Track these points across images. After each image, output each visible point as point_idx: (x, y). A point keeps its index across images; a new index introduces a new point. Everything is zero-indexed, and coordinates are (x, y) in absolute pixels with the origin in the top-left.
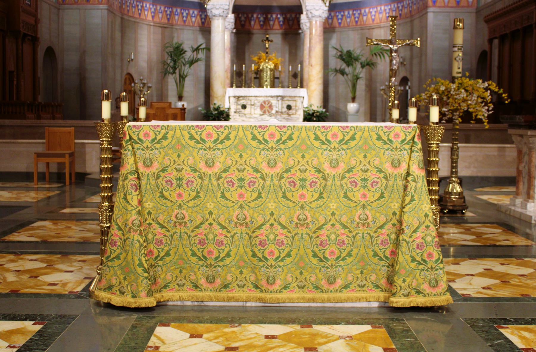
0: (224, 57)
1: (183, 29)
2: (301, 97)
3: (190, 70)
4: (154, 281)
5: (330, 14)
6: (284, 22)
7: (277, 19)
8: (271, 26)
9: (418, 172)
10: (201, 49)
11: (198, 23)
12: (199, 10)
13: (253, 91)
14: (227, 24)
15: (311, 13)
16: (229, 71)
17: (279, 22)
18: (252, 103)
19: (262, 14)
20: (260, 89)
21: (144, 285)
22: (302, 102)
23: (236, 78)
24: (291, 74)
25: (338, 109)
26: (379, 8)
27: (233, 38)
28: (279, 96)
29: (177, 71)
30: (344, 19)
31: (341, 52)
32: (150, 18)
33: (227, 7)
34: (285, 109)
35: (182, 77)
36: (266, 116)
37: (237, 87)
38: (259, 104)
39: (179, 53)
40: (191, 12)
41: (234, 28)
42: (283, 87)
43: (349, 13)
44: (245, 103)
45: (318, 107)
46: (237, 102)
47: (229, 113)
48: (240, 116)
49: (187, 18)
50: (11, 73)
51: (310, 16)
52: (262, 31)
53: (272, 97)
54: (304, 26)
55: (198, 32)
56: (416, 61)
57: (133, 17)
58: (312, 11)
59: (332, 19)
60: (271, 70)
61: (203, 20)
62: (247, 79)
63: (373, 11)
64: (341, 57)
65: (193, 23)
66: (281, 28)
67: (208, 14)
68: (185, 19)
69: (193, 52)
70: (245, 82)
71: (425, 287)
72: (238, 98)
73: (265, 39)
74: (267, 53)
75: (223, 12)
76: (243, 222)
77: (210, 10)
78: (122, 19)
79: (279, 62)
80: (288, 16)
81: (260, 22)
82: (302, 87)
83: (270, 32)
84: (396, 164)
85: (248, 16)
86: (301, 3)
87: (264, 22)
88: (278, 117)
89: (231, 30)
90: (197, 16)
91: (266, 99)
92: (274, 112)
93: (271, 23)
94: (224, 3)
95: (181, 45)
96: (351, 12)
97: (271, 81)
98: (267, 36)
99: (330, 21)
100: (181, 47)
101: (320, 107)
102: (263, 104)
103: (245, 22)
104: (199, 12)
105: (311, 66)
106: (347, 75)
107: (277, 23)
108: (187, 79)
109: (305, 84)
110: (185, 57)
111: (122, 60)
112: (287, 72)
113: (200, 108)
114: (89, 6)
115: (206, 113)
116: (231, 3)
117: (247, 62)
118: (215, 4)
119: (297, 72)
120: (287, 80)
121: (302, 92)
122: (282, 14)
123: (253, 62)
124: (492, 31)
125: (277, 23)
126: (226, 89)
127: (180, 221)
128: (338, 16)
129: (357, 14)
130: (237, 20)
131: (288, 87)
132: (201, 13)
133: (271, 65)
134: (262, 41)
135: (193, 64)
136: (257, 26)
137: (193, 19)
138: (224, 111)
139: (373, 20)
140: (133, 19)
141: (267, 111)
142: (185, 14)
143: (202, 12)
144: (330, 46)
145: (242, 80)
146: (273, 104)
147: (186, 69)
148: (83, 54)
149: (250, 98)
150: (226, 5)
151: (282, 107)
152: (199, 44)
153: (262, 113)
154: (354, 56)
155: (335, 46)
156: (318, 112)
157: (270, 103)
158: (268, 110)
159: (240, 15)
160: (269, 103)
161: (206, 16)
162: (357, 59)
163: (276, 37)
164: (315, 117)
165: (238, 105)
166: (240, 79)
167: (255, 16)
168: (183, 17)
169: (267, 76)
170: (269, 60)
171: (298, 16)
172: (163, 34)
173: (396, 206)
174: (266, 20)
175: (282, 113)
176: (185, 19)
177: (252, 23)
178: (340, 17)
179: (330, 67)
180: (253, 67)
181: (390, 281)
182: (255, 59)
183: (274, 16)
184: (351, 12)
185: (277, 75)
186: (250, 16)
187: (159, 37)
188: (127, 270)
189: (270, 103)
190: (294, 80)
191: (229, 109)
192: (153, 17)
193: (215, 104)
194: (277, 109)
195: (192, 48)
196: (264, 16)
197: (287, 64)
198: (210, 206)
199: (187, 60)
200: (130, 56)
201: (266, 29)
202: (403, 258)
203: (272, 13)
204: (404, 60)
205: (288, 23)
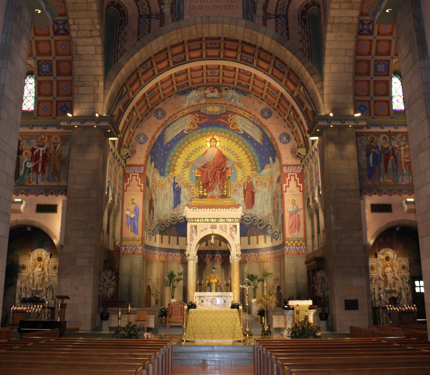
4: (194, 336)
6: (222, 258)
7: (218, 257)
9: (238, 317)
13: (207, 294)
17: (219, 258)
19: (211, 254)
20: (211, 293)
21: (192, 337)
29: (171, 284)
32: (158, 258)
42: (221, 291)
50: (405, 347)
52: (211, 263)
53: (216, 296)
56: (282, 279)
57: (151, 258)
59: (245, 257)
60: (216, 283)
63: (264, 253)
64: (248, 277)
66: (221, 261)
71: (239, 337)
72: (200, 297)
76: (209, 326)
78: (147, 260)
80: (224, 255)
82: (231, 291)
83: (215, 263)
84: (234, 316)
87: (212, 258)
91: (214, 297)
93: (216, 259)
103: (203, 258)
107: (218, 258)
108: (176, 289)
111: (146, 279)
114: (134, 256)
121: (231, 294)
122: (221, 254)
123: (207, 279)
124: (308, 268)
125: (218, 258)
127: (198, 326)
129: (257, 254)
130: (199, 257)
133: (215, 281)
136: (209, 260)
137: (178, 258)
139: (264, 258)
140: (150, 260)
142: (174, 255)
147: (175, 284)
148: (131, 277)
162: (256, 278)
163: (218, 266)
165: (200, 300)
167: (208, 255)
169: (214, 286)
170: (215, 278)
172: (163, 266)
173: (234, 323)
174: (213, 257)
177: (206, 259)
180: (207, 282)
181: (234, 336)
182: (208, 278)
183: (217, 255)
187: (162, 267)
188: (190, 334)
192: (159, 258)
198: (203, 324)
200: (149, 277)
201: (213, 262)
202: (236, 332)
204: (278, 278)
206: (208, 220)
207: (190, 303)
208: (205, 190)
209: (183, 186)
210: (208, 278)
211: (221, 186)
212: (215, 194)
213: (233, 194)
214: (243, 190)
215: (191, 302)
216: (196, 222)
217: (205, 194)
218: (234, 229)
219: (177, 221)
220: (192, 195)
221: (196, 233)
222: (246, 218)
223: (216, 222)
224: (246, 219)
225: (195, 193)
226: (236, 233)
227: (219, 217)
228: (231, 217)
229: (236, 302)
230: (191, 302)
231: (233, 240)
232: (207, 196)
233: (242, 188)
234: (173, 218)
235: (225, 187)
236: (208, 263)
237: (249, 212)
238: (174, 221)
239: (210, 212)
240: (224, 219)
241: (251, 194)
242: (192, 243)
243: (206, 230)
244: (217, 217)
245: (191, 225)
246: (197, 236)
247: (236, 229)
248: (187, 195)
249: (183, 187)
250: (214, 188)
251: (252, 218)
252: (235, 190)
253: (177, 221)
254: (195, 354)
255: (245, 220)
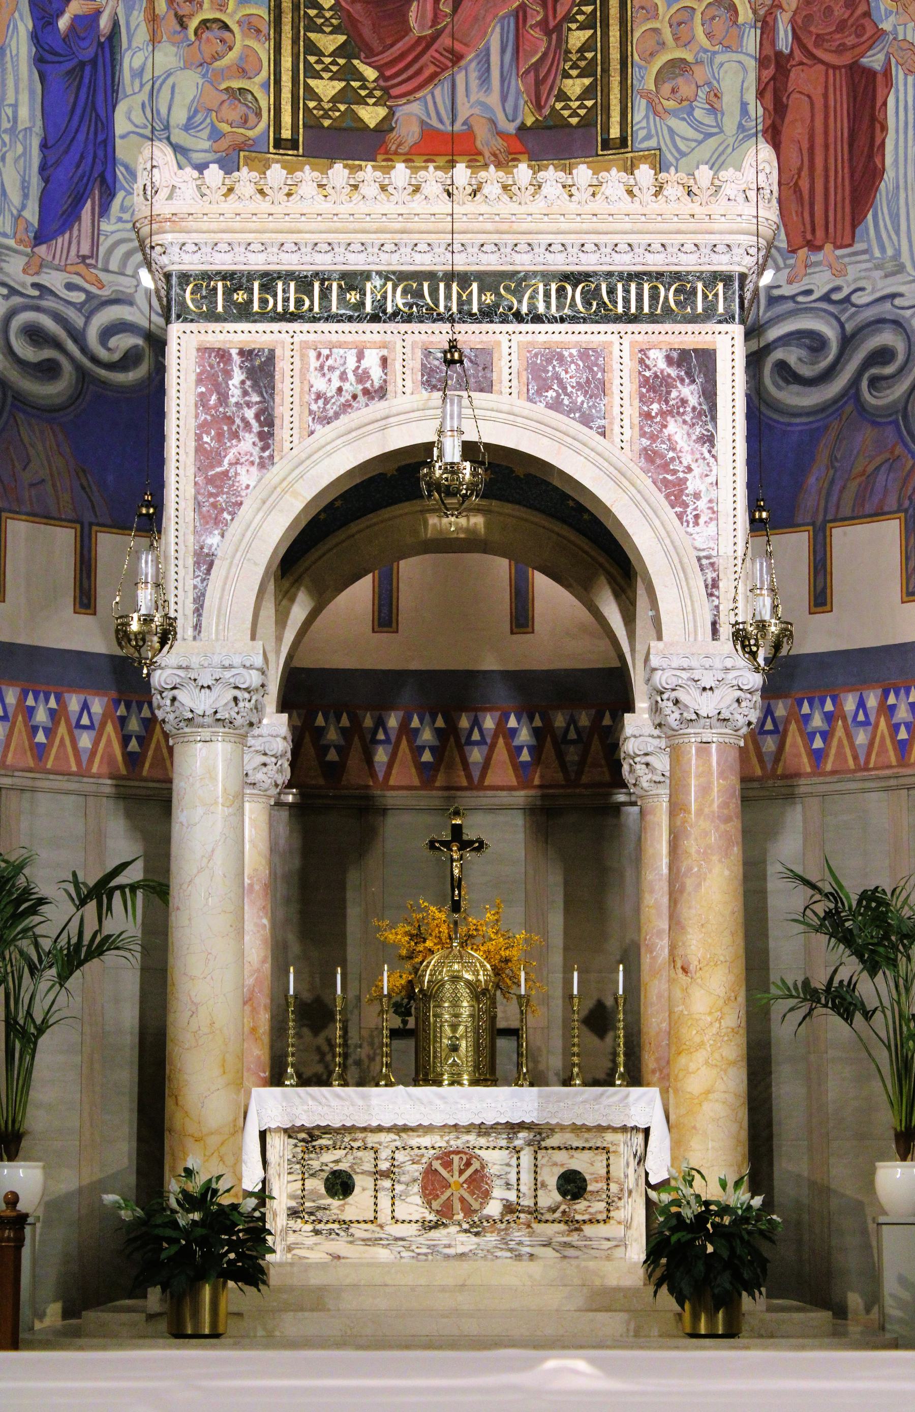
0: (240, 932)
1: (34, 790)
2: (635, 1129)
3: (62, 998)
5: (768, 712)
6: (536, 750)
8: (476, 774)
10: (121, 888)
11: (110, 759)
12: (114, 694)
14: (252, 761)
15: (676, 702)
16: (263, 999)
18: (384, 1166)
22: (641, 1160)
23: (298, 1035)
24: (580, 1009)
25: (822, 1191)
26: (850, 704)
27: (283, 830)
28: (522, 1126)
30: (840, 732)
31: (833, 896)
33: (254, 679)
34: (551, 1197)
35: (23, 1034)
36: (453, 1229)
37: (304, 1081)
38: (415, 1170)
39: (10, 910)
40: (74, 703)
41: (290, 785)
43: (861, 704)
44: (343, 1166)
45: (723, 1185)
46: (302, 1162)
47: (263, 1218)
48: (317, 1232)
49: (49, 732)
51: (673, 718)
52: (433, 798)
53: (482, 1129)
54: (640, 769)
55: (108, 805)
58: (680, 694)
59: (780, 732)
60: (478, 993)
61: (133, 745)
62: (354, 1039)
65: (84, 758)
66: (524, 783)
67: (160, 714)
68: (41, 737)
69: (83, 902)
70: (345, 1056)
73: (446, 836)
74: (456, 907)
75: (235, 699)
77: (168, 695)
79: (515, 953)
81: (417, 751)
82: (635, 1078)
83: (467, 799)
85: (356, 721)
86: (621, 657)
88: (518, 1234)
89: (274, 791)
90: (103, 725)
92: (494, 1209)
93: (476, 755)
94: (237, 661)
95: (19, 868)
96: (872, 702)
97: (477, 1046)
98: (458, 822)
99: (769, 744)
100: (21, 881)
101: (737, 1184)
102: (437, 1165)
104: (117, 703)
105: (685, 970)
106: (868, 1015)
107: (501, 752)
109: (649, 1061)
110: (38, 930)
112: (558, 1003)
113: (110, 1198)
115: (139, 1222)
116: (272, 657)
117: (352, 954)
118: (195, 661)
119: (609, 1002)
120: (557, 1043)
122: (527, 712)
123: (386, 952)
125: (501, 752)
126: (248, 1094)
128: (807, 718)
131: (567, 1082)
132: (122, 711)
134: (432, 845)
135: (81, 963)
138: (234, 1207)
141: (457, 1205)
143: (128, 707)
144: (773, 869)
145: (331, 1045)
146: (493, 1170)
149: (372, 1139)
150: (251, 667)
151: (538, 1185)
152: (110, 866)
153: (432, 1217)
154: (901, 920)
155: (799, 870)
156: (725, 1210)
157: (476, 1165)
158: (462, 1200)
159: (320, 721)
160: (468, 1164)
161: (150, 723)
164: (710, 1238)
166: (321, 1040)
168: (34, 730)
170: (467, 940)
171: (607, 721)
175: (535, 1212)
176: (41, 737)
177: (381, 756)
178: (817, 722)
179: (774, 977)
184: (872, 702)
185: (507, 1015)
186: (368, 722)
189: (476, 1165)
190: (592, 1040)
191: (263, 1196)
193: (189, 1173)
194: (512, 1196)
195: (76, 883)
196: (440, 723)
197: (557, 958)
199: (46, 944)
203: (476, 710)
205: (560, 756)
206: (397, 300)
207: (190, 1201)
208: (370, 74)
209: (138, 17)
210: (398, 936)
211: (536, 37)
212: (464, 112)
213: (653, 108)
214: (762, 62)
215: (209, 1191)
216: (266, 316)
217: (371, 115)
218: (689, 393)
219: (82, 373)
220: (233, 112)
221: (266, 437)
222: (786, 340)
223: (487, 314)
224: (792, 356)
225: (265, 102)
226: (709, 440)
227: (523, 262)
228: (656, 262)
229: (710, 1190)
230: (209, 1191)
231: (669, 514)
232: (385, 128)
233: (751, 41)
234: (34, 334)
235: (577, 38)
236: (392, 798)
237: (821, 282)
238: (48, 370)
239: (417, 205)
240: (573, 278)
241: (840, 101)
242: (213, 540)
243: (378, 407)
244: (491, 262)
245: (204, 351)
246: (276, 472)
247: (709, 394)
248: (179, 116)
249: (142, 35)
250: (457, 58)
251: (848, 341)
252: (678, 67)
253: (82, 373)
254: (460, 767)
255: (782, 367)
